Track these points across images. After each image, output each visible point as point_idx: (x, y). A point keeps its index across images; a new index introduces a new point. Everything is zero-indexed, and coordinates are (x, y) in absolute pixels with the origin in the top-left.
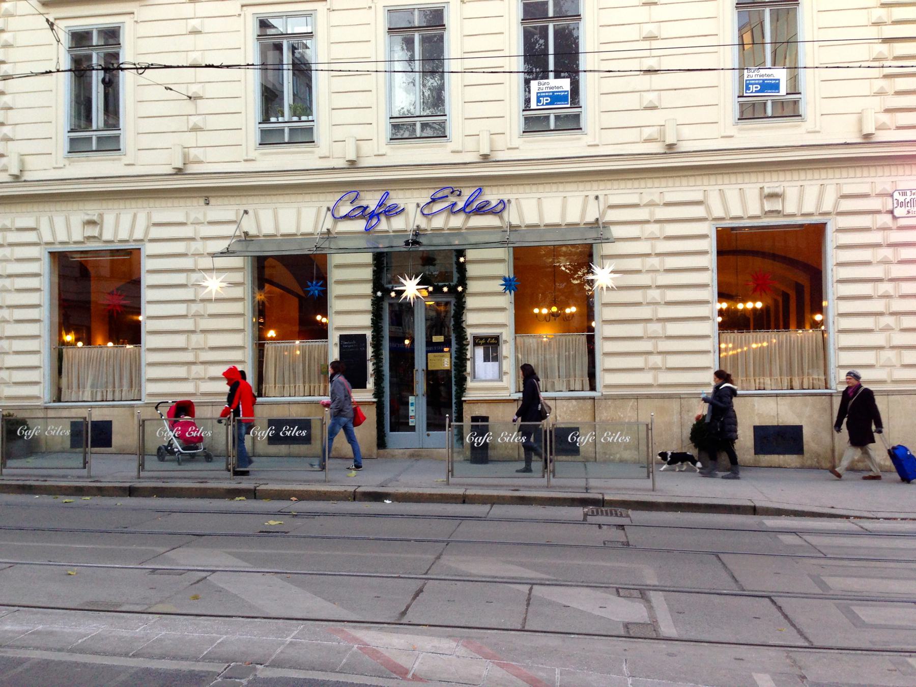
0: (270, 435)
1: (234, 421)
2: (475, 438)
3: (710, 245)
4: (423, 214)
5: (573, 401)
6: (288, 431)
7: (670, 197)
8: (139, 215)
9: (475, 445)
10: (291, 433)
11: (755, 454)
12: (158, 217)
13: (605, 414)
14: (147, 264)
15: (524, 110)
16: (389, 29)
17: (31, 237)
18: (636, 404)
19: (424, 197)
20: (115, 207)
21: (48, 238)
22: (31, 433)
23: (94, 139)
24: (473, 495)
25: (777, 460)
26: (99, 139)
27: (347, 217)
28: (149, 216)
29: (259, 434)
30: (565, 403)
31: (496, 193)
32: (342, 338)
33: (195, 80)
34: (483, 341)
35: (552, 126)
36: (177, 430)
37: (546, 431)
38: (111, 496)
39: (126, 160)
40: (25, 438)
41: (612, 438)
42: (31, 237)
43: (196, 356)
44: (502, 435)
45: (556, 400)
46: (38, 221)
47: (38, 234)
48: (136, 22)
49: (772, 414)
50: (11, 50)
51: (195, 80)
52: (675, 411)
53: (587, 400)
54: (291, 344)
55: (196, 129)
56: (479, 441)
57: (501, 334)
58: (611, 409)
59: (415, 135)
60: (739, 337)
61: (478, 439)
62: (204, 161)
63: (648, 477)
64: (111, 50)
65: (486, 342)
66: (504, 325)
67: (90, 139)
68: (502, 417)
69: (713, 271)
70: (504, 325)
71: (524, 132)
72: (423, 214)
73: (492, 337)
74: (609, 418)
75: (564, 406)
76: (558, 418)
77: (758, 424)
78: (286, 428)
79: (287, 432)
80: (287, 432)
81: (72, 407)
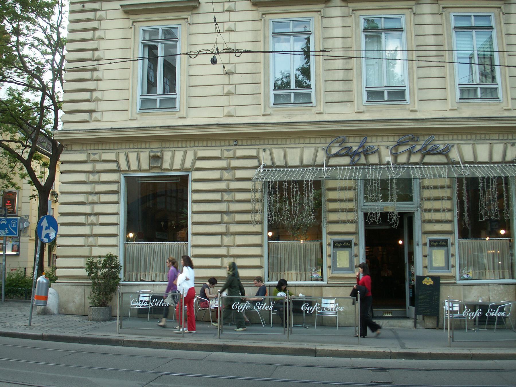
0: (246, 308)
5: (501, 286)
6: (157, 302)
9: (308, 312)
10: (262, 308)
12: (201, 153)
14: (192, 186)
15: (273, 90)
19: (392, 141)
20: (172, 146)
22: (312, 309)
23: (292, 95)
24: (478, 354)
26: (161, 100)
27: (336, 155)
28: (195, 154)
29: (308, 309)
30: (495, 287)
31: (438, 139)
33: (229, 62)
37: (286, 303)
39: (178, 115)
40: (238, 311)
41: (261, 306)
43: (228, 251)
46: (118, 156)
47: (117, 164)
48: (189, 24)
50: (102, 42)
51: (229, 62)
55: (229, 94)
56: (472, 315)
59: (291, 102)
61: (310, 308)
62: (234, 115)
63: (285, 333)
67: (289, 95)
71: (460, 99)
75: (495, 289)
76: (491, 298)
78: (155, 300)
79: (259, 307)
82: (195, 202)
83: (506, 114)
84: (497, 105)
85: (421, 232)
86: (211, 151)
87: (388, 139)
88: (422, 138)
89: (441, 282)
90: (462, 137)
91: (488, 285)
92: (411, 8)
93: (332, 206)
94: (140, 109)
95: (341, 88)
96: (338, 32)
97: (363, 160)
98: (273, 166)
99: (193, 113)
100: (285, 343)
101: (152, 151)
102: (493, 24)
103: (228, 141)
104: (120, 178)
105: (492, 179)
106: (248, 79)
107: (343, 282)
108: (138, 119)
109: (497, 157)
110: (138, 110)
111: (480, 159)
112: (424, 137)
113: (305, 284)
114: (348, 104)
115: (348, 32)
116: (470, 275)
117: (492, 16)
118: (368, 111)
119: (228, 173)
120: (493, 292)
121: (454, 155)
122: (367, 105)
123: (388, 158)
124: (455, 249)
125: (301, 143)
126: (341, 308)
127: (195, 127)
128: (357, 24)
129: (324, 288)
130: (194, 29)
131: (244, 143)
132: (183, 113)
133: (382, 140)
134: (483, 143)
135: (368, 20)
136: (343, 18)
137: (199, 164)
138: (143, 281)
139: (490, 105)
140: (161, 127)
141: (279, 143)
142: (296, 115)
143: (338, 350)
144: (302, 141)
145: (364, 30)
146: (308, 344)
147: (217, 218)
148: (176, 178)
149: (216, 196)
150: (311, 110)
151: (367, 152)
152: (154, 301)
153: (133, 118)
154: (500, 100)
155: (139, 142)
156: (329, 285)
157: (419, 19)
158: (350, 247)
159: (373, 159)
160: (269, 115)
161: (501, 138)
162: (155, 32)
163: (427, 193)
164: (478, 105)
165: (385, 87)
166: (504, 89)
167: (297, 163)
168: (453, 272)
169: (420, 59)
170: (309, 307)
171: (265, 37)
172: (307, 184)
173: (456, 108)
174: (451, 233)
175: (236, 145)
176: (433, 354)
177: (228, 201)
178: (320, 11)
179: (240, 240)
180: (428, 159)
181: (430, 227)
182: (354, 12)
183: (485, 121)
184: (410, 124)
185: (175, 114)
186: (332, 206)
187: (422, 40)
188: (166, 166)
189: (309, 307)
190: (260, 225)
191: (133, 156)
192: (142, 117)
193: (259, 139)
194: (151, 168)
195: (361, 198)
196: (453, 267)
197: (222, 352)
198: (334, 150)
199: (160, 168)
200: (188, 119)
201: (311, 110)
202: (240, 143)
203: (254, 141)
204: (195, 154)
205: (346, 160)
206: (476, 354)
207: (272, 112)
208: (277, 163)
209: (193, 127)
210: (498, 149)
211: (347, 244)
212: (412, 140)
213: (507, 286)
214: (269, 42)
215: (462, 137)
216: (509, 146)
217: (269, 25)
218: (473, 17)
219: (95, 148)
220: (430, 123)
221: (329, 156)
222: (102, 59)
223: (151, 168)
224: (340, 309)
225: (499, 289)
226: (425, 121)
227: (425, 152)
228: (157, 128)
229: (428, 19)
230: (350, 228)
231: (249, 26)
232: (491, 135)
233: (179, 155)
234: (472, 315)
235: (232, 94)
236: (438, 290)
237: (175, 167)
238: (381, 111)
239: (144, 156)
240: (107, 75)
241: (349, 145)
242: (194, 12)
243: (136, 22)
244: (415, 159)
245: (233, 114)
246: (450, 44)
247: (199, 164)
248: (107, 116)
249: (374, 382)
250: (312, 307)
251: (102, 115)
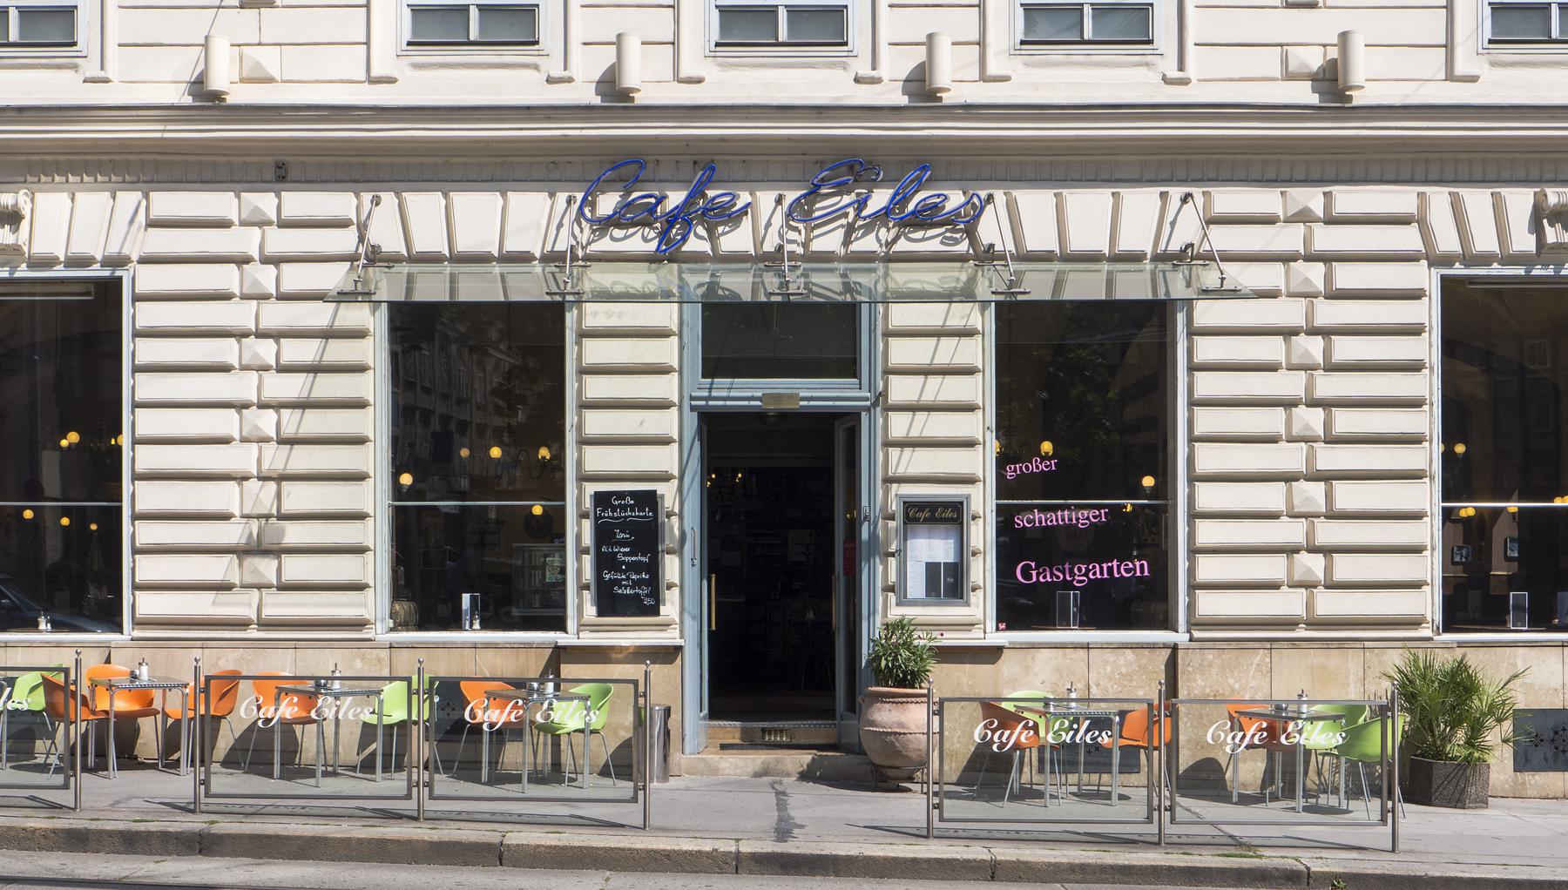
2: (994, 731)
3: (1428, 312)
5: (1128, 651)
11: (1515, 770)
13: (1200, 682)
14: (137, 316)
17: (1407, 239)
18: (1268, 660)
21: (1448, 241)
32: (601, 499)
34: (926, 514)
35: (783, 35)
36: (516, 706)
38: (150, 852)
40: (995, 748)
42: (1407, 239)
45: (1088, 648)
49: (1552, 685)
52: (1352, 677)
53: (1158, 651)
56: (1004, 739)
57: (968, 497)
58: (1214, 670)
59: (777, 39)
61: (1002, 734)
66: (970, 481)
68: (969, 686)
69: (1431, 369)
70: (970, 481)
74: (1208, 690)
79: (1063, 734)
91: (1087, 647)
93: (597, 387)
113: (507, 640)
120: (1102, 672)
121: (992, 230)
122: (1022, 52)
126: (1104, 734)
170: (1000, 731)
186: (597, 387)
189: (1000, 731)
205: (639, 241)
206: (1007, 861)
208: (1033, 244)
211: (948, 514)
213: (1146, 652)
224: (1099, 739)
234: (1004, 739)
250: (1007, 733)
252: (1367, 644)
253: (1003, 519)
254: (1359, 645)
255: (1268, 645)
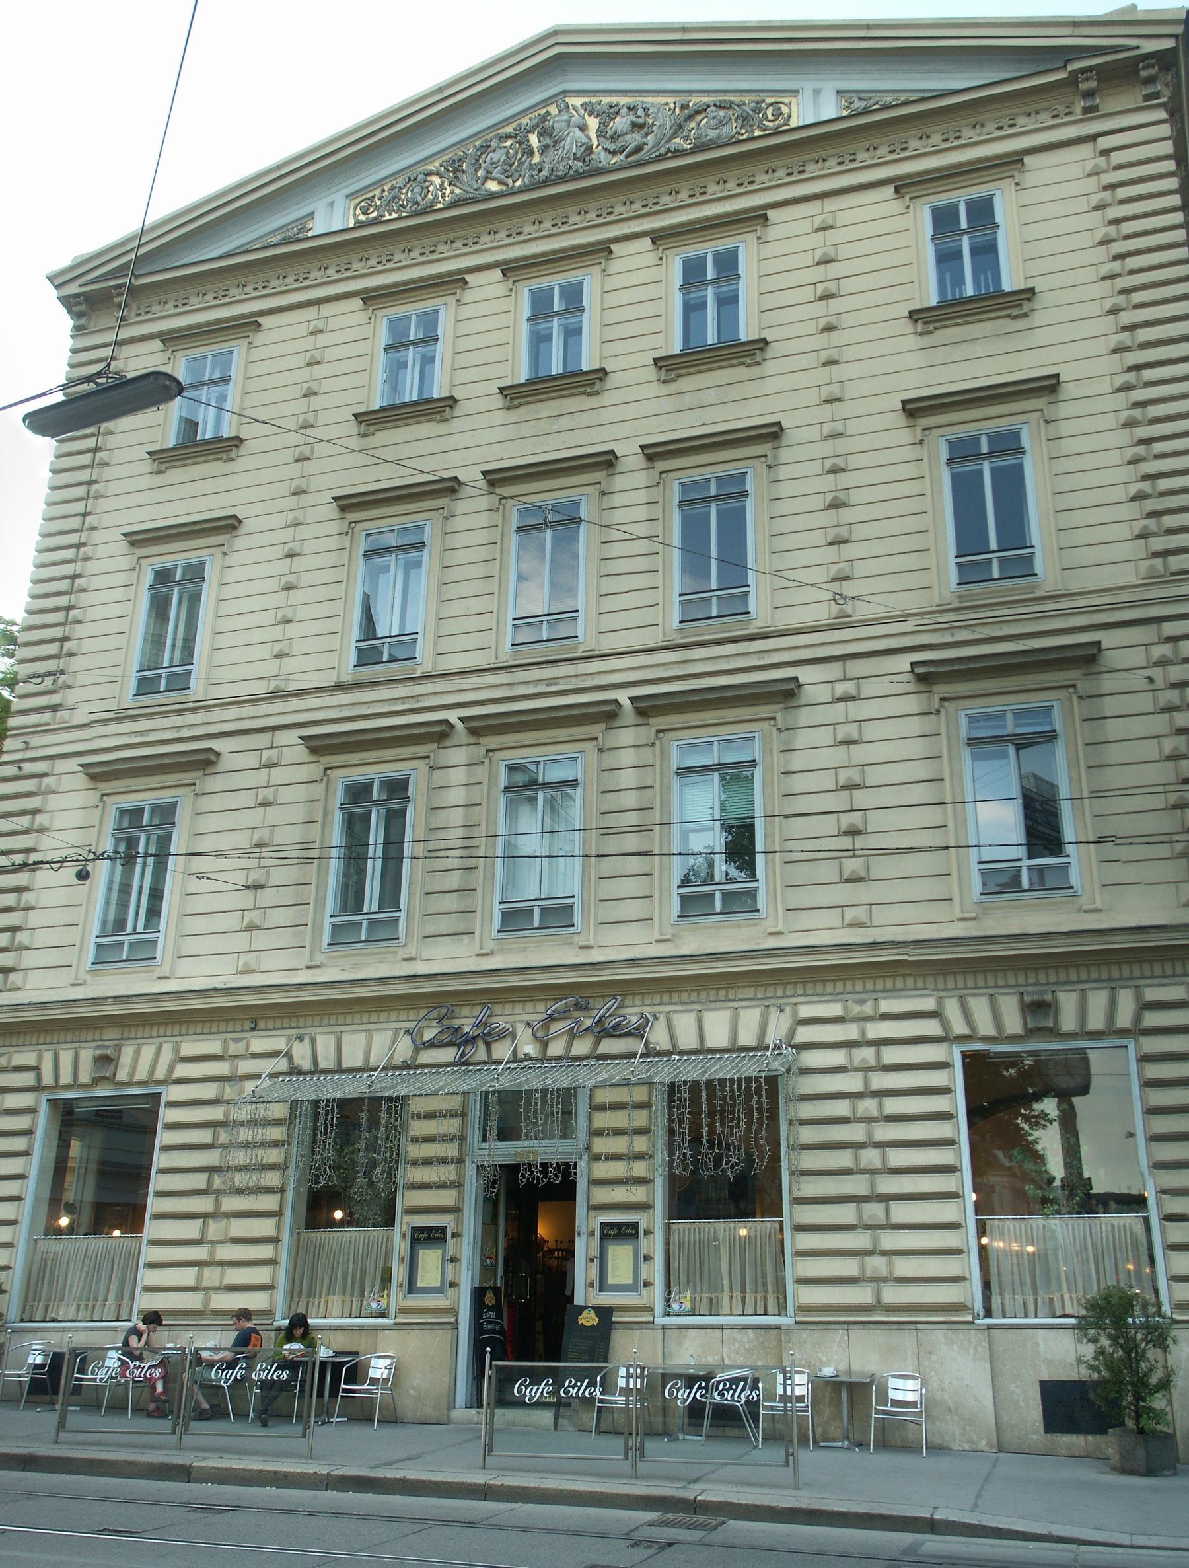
1: (491, 1369)
4: (536, 1037)
7: (886, 1006)
8: (165, 1046)
10: (578, 1391)
11: (1046, 1432)
12: (188, 1049)
14: (167, 1115)
16: (969, 739)
17: (931, 1027)
18: (846, 1338)
19: (536, 1012)
20: (140, 1035)
21: (960, 1028)
23: (718, 896)
25: (1083, 1444)
27: (432, 1044)
28: (177, 1049)
29: (528, 1393)
30: (736, 1334)
34: (615, 1231)
35: (718, 908)
36: (700, 1387)
39: (159, 972)
40: (679, 1403)
44: (566, 1385)
49: (1068, 1361)
54: (338, 1234)
55: (251, 928)
56: (533, 1394)
60: (1023, 1227)
63: (787, 1464)
64: (395, 805)
65: (619, 1232)
67: (711, 895)
71: (679, 917)
72: (536, 1037)
73: (437, 1229)
75: (735, 1340)
77: (1046, 1378)
78: (570, 1382)
79: (725, 1392)
80: (725, 1392)
81: (63, 1330)
82: (167, 1148)
83: (772, 943)
84: (755, 925)
85: (585, 1204)
86: (917, 1000)
87: (535, 1007)
88: (599, 1003)
89: (614, 1319)
90: (680, 997)
92: (774, 718)
94: (499, 932)
95: (455, 907)
96: (457, 796)
97: (481, 1054)
98: (316, 1071)
99: (185, 967)
100: (171, 1453)
101: (98, 1047)
102: (1058, 725)
103: (241, 1022)
104: (37, 1101)
105: (680, 1086)
106: (289, 896)
107: (423, 1321)
108: (88, 982)
109: (747, 1038)
110: (89, 966)
111: (710, 1043)
112: (513, 1006)
114: (466, 937)
115: (477, 794)
116: (687, 1305)
117: (1055, 707)
118: (501, 951)
119: (231, 1087)
121: (659, 1037)
123: (530, 1049)
124: (655, 1245)
125: (371, 1020)
127: (176, 995)
128: (492, 777)
129: (381, 1334)
130: (206, 803)
131: (270, 1024)
132: (165, 970)
133: (523, 1009)
134: (719, 1009)
135: (512, 769)
136: (471, 767)
137: (182, 1071)
138: (54, 1320)
139: (739, 927)
140: (115, 997)
141: (332, 1022)
142: (368, 964)
143: (231, 1469)
144: (374, 1017)
145: (505, 788)
146: (197, 1454)
147: (199, 1181)
148: (144, 1101)
149: (204, 1136)
150: (396, 953)
151: (488, 1038)
152: (721, 1388)
153: (483, 951)
154: (1075, 890)
155: (162, 1023)
156: (398, 1326)
157: (609, 760)
158: (444, 1240)
159: (502, 1051)
160: (318, 967)
161: (759, 996)
162: (139, 812)
163: (603, 1120)
164: (716, 928)
165: (536, 900)
166: (771, 891)
167: (359, 1064)
168: (645, 1297)
169: (432, 855)
171: (325, 814)
172: (327, 1106)
173: (669, 937)
174: (646, 1207)
175: (253, 1029)
176: (409, 1481)
177: (224, 1147)
178: (428, 757)
179: (239, 1228)
180: (607, 1046)
181: (603, 1195)
182: (661, 735)
183: (717, 960)
184: (569, 974)
185: (153, 971)
187: (612, 801)
188: (122, 1076)
190: (278, 1196)
191: (66, 1057)
192: (96, 978)
193: (1045, 968)
194: (96, 1082)
195: (475, 1135)
196: (646, 1284)
197: (24, 1470)
198: (428, 1035)
199: (111, 1080)
200: (173, 980)
201: (396, 953)
202: (262, 1024)
203: (762, 989)
204: (177, 1049)
205: (448, 1055)
207: (325, 961)
209: (172, 996)
210: (750, 1019)
212: (578, 1006)
214: (332, 823)
215: (680, 997)
216: (773, 1012)
217: (336, 788)
218: (1009, 715)
219: (701, 997)
220: (608, 972)
221: (419, 1047)
222: (267, 845)
223: (1030, 1033)
225: (745, 1339)
226: (598, 967)
227: (604, 1031)
228: (109, 1000)
229: (627, 757)
230: (446, 1198)
231: (301, 792)
232: (740, 990)
233: (148, 1052)
234: (533, 1394)
235: (258, 928)
236: (606, 1339)
237: (137, 1077)
238: (524, 950)
239: (87, 1056)
240: (46, 898)
241: (456, 1023)
242: (207, 772)
243: (107, 795)
244: (582, 1047)
245: (253, 967)
246: (666, 805)
247: (182, 1071)
248: (35, 979)
249: (112, 1530)
250: (230, 1372)
251: (258, 958)
252: (919, 1326)
253: (1100, 1206)
254: (912, 1326)
255: (845, 1326)
